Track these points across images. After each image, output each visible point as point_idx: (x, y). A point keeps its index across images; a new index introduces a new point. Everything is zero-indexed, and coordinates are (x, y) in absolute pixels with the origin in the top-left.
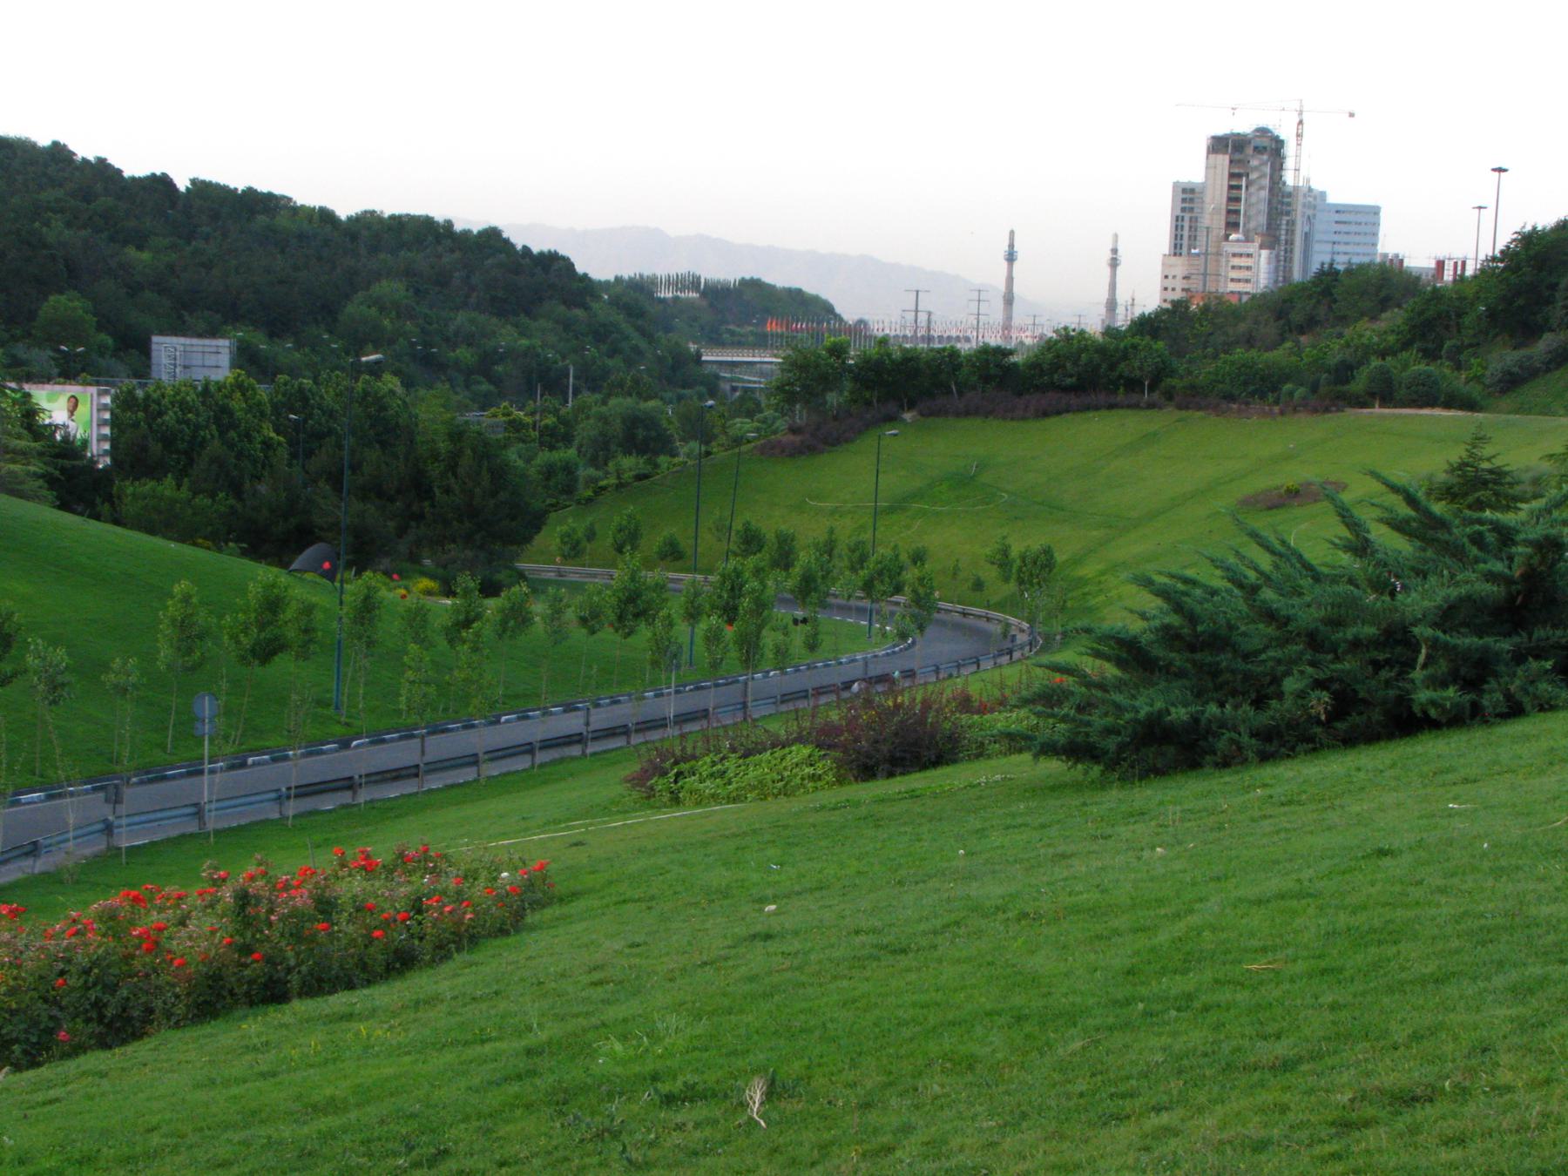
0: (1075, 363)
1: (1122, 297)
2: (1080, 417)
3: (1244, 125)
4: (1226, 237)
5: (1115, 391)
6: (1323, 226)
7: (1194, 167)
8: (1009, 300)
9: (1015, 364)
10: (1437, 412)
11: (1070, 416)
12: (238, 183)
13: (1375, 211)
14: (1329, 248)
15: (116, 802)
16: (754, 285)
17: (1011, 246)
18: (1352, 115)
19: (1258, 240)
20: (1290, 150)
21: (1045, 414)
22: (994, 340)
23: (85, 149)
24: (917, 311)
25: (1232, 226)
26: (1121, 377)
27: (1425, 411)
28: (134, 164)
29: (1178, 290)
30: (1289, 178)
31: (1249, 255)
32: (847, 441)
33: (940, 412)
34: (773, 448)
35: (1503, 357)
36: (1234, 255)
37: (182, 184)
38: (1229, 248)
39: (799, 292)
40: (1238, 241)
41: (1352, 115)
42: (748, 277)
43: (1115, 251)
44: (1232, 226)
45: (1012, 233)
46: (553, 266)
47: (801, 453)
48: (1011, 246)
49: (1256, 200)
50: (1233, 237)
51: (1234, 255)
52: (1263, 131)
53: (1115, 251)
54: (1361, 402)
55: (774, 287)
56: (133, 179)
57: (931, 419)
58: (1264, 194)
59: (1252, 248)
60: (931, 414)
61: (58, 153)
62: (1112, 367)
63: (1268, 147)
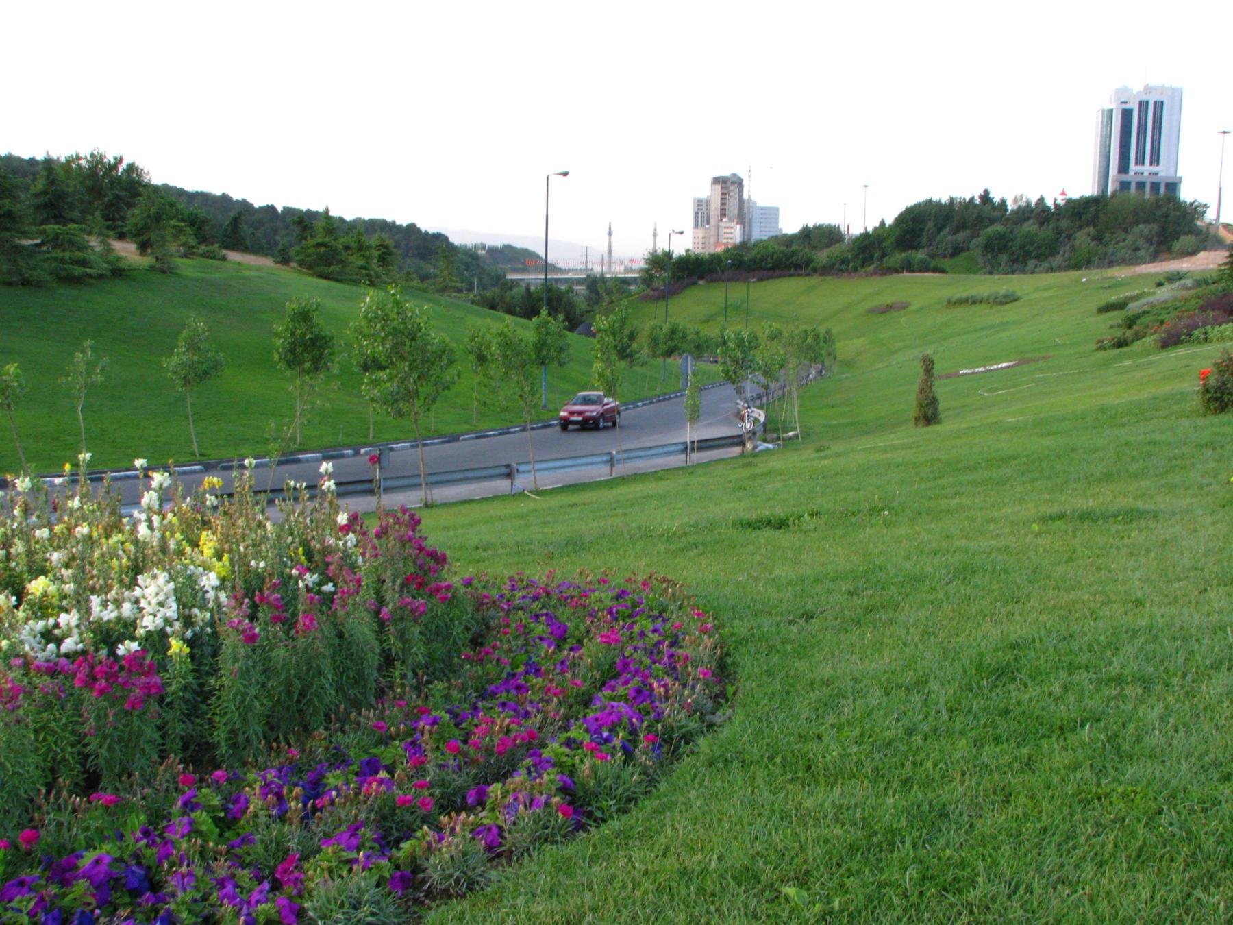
1: (616, 254)
3: (726, 173)
6: (756, 217)
7: (705, 190)
8: (610, 252)
10: (931, 274)
12: (304, 208)
13: (777, 209)
18: (565, 174)
20: (745, 183)
21: (761, 279)
22: (597, 269)
23: (236, 196)
25: (723, 215)
27: (926, 274)
28: (258, 201)
30: (745, 196)
33: (712, 281)
35: (898, 257)
37: (280, 209)
38: (722, 224)
41: (565, 174)
44: (723, 215)
46: (439, 239)
49: (732, 203)
52: (734, 175)
54: (897, 271)
56: (261, 208)
57: (714, 284)
58: (736, 202)
59: (733, 224)
61: (225, 198)
62: (787, 259)
63: (738, 182)
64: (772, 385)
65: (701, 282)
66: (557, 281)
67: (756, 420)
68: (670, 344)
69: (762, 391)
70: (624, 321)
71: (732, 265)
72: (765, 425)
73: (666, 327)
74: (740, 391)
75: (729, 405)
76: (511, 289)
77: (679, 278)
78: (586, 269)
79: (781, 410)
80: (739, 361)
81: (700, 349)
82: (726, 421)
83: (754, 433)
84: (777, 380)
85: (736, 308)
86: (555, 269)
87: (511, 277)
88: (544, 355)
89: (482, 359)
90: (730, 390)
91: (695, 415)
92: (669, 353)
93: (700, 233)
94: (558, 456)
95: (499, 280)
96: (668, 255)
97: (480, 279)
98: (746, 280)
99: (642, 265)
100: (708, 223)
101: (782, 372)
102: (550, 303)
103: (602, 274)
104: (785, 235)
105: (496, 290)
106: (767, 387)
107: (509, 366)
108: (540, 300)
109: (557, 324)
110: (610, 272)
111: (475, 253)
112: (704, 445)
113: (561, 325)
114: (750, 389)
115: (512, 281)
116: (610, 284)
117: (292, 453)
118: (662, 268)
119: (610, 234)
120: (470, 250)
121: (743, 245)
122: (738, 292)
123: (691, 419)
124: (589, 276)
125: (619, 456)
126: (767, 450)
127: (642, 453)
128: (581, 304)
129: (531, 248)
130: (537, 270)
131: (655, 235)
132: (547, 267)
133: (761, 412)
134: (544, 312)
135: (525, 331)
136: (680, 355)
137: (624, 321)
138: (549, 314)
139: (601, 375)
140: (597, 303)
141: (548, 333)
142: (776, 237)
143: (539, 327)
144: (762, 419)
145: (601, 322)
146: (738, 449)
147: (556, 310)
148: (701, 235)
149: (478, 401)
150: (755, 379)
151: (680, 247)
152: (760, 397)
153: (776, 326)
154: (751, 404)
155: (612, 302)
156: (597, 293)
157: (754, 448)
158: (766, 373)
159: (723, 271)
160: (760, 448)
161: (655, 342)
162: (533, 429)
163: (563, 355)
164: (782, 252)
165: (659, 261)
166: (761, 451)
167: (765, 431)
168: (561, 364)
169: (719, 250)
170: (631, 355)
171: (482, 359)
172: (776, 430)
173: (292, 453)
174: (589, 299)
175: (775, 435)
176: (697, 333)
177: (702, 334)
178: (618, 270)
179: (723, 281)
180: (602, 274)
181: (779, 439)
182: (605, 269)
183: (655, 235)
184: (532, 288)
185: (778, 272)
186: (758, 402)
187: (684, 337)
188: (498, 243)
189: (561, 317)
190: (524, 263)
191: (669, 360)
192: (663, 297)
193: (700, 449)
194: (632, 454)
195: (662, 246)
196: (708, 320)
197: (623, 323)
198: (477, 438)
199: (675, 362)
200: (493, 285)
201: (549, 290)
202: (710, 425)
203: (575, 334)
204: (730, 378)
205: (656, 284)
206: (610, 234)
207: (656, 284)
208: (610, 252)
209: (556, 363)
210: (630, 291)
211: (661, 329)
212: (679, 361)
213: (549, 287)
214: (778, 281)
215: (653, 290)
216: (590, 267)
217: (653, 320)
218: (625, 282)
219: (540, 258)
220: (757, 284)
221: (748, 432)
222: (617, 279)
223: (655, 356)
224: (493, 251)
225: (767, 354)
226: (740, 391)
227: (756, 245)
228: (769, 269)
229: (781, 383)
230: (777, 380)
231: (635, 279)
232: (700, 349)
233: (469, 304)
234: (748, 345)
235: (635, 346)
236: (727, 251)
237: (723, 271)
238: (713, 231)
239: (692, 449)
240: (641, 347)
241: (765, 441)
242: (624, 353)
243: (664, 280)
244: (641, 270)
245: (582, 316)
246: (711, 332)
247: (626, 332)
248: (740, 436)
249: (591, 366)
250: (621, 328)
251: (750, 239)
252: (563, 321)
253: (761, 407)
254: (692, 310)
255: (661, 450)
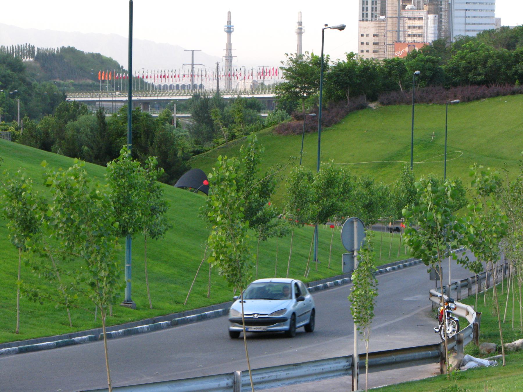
0: (484, 65)
2: (493, 101)
4: (404, 7)
5: (513, 83)
8: (229, 58)
9: (440, 69)
11: (486, 100)
14: (462, 13)
15: (438, 279)
16: (71, 51)
17: (229, 22)
19: (426, 8)
21: (467, 100)
22: (210, 86)
24: (193, 64)
26: (516, 73)
29: (371, 44)
31: (420, 19)
32: (336, 123)
34: (287, 129)
36: (409, 19)
38: (406, 14)
39: (99, 55)
40: (411, 9)
42: (66, 46)
43: (300, 23)
45: (229, 13)
47: (307, 131)
48: (229, 22)
50: (408, 7)
51: (409, 19)
53: (300, 23)
55: (82, 52)
57: (389, 107)
59: (423, 13)
60: (389, 103)
62: (509, 67)
64: (487, 266)
65: (372, 105)
66: (146, 103)
67: (462, 321)
68: (327, 203)
69: (470, 274)
70: (252, 166)
71: (422, 77)
72: (476, 328)
73: (319, 176)
74: (435, 276)
75: (419, 297)
76: (73, 117)
77: (339, 98)
78: (194, 86)
79: (502, 304)
80: (437, 229)
81: (372, 209)
82: (420, 326)
83: (460, 342)
84: (494, 258)
85: (428, 145)
86: (143, 86)
87: (73, 98)
88: (130, 220)
89: (28, 226)
90: (421, 272)
91: (367, 312)
92: (324, 217)
93: (371, 27)
94: (152, 380)
95: (54, 103)
96: (320, 62)
97: (25, 102)
98: (443, 101)
99: (280, 78)
100: (383, 13)
101: (503, 244)
102: (135, 137)
103: (218, 93)
104: (505, 29)
105: (51, 119)
106: (478, 269)
107: (75, 235)
108: (121, 134)
109: (145, 172)
110: (229, 90)
111: (18, 61)
112: (380, 360)
113: (154, 174)
114: (452, 271)
115: (77, 104)
116: (229, 109)
117: (71, 336)
118: (312, 84)
119: (229, 30)
120: (9, 55)
121: (439, 46)
122: (432, 118)
123: (360, 320)
124: (196, 97)
125: (247, 379)
126: (481, 367)
127: (282, 374)
128: (185, 142)
129: (106, 53)
130: (116, 87)
131: (300, 32)
132: (131, 83)
133: (470, 309)
134: (125, 152)
135: (99, 182)
136: (341, 219)
137: (252, 166)
138: (134, 156)
139: (220, 249)
140: (210, 138)
141: (132, 186)
142: (490, 32)
143: (119, 175)
144: (472, 319)
145: (223, 167)
146: (434, 367)
147: (146, 152)
148: (372, 31)
149: (25, 291)
150: (460, 256)
151: (339, 51)
152: (467, 284)
153: (493, 172)
154: (454, 295)
155: (233, 137)
156: (209, 122)
157: (461, 364)
158: (476, 246)
159: (407, 87)
160: (470, 365)
161: (300, 199)
162: (109, 336)
163: (158, 219)
164: (500, 56)
165: (307, 74)
166: (470, 370)
167: (476, 337)
168: (153, 235)
169: (401, 54)
170: (264, 220)
171: (28, 226)
172: (493, 337)
173: (71, 336)
174: (196, 132)
175: (493, 345)
176: (368, 185)
177: (374, 187)
178: (242, 87)
179: (408, 103)
180: (218, 93)
181: (499, 350)
182: (222, 86)
183: (300, 32)
184: (108, 116)
185: (494, 88)
186: (465, 292)
187: (347, 190)
188: (53, 44)
189: (153, 160)
190: (95, 77)
191: (323, 228)
192: (314, 129)
193: (374, 367)
194: (266, 376)
195: (311, 49)
196: (385, 163)
197: (251, 171)
198: (21, 351)
199: (333, 230)
200: (48, 112)
201: (135, 118)
202: (387, 329)
203: (175, 188)
204: (424, 254)
205: (302, 108)
206: (229, 30)
207: (302, 108)
208: (229, 58)
209: (145, 232)
210: (261, 120)
211: (310, 179)
212: (339, 229)
213: (133, 114)
214: (493, 101)
215: (298, 118)
216: (198, 82)
217: (296, 165)
218: (253, 105)
219: (120, 69)
220: (460, 107)
221: (450, 340)
222: (240, 101)
223: (301, 222)
224: (46, 58)
225: (478, 217)
226: (435, 276)
227: (458, 45)
228: (480, 83)
229: (501, 262)
230: (494, 258)
231: (269, 100)
232: (372, 209)
233: (8, 142)
234: (451, 202)
235: (269, 206)
236: (414, 55)
237: (407, 87)
238: (390, 25)
239: (362, 368)
240: (280, 205)
241: (477, 354)
242: (256, 217)
243: (315, 102)
244: (279, 87)
245: (186, 159)
246: (389, 182)
247: (256, 184)
248: (438, 346)
249: (206, 236)
250: (249, 176)
251: (449, 37)
252: (157, 167)
253: (469, 301)
254: (359, 148)
255: (312, 369)
